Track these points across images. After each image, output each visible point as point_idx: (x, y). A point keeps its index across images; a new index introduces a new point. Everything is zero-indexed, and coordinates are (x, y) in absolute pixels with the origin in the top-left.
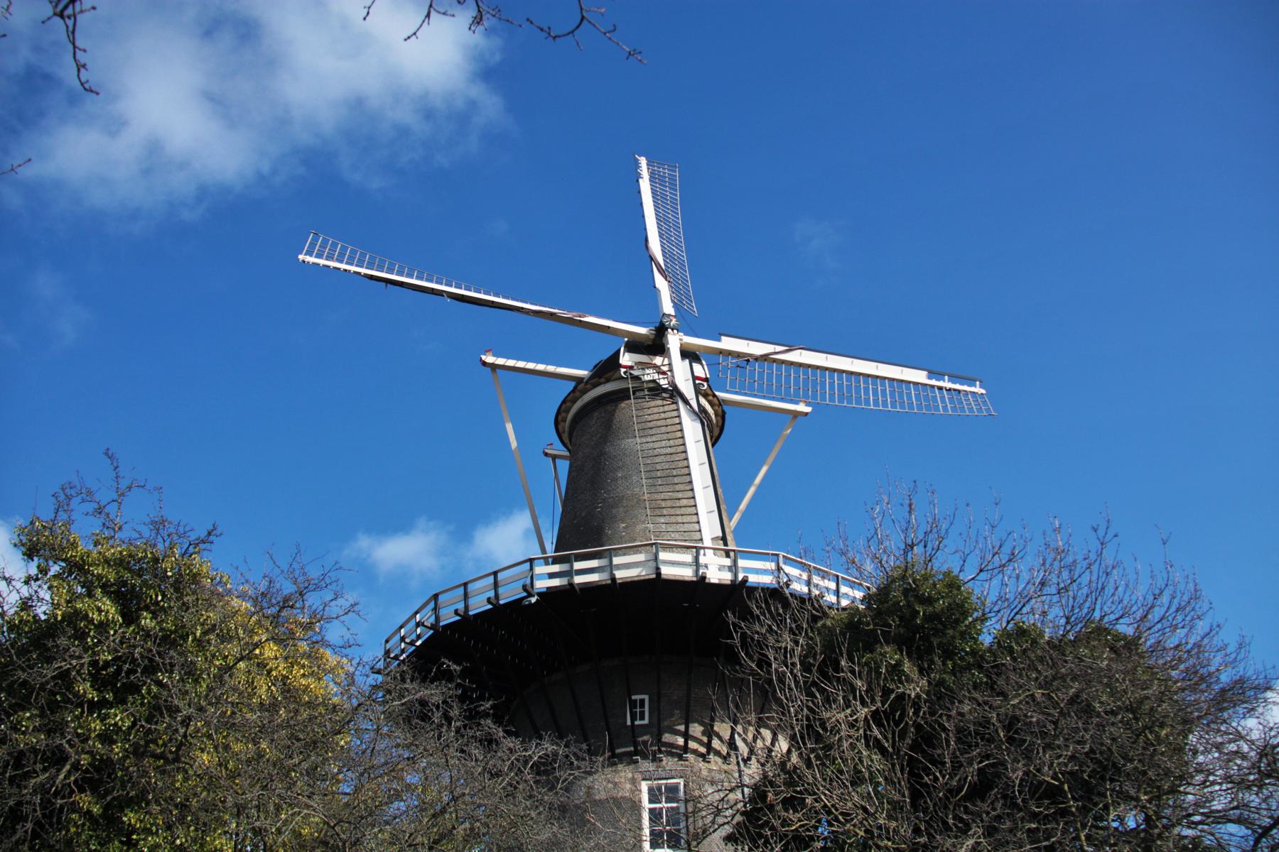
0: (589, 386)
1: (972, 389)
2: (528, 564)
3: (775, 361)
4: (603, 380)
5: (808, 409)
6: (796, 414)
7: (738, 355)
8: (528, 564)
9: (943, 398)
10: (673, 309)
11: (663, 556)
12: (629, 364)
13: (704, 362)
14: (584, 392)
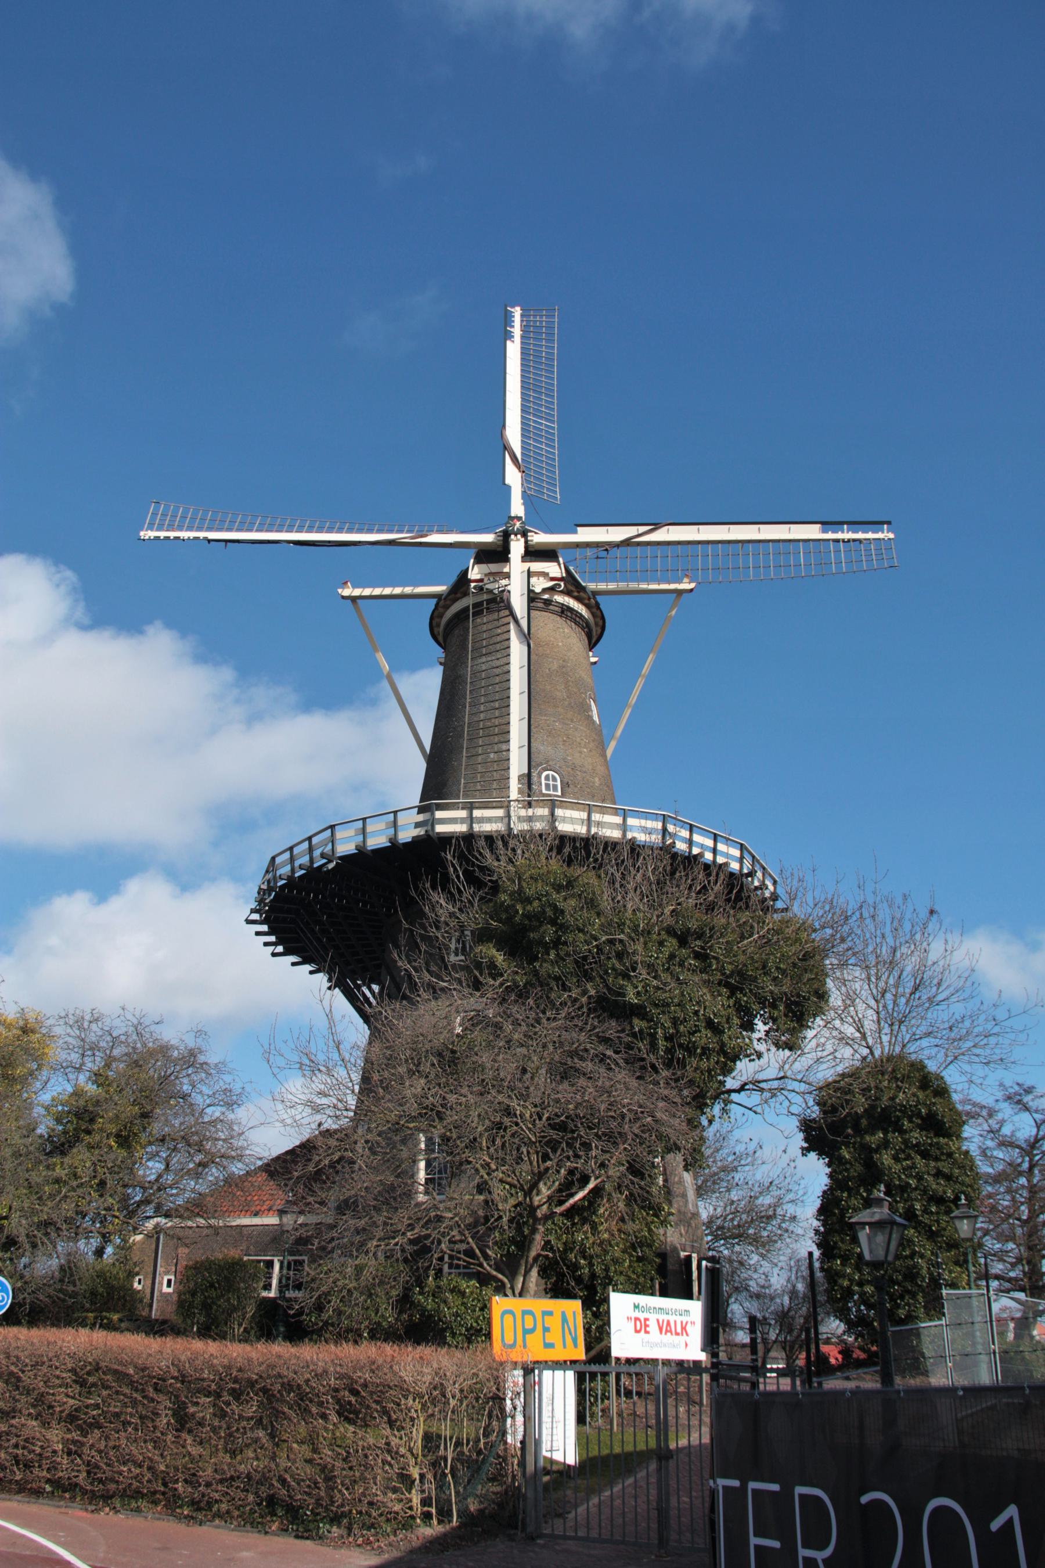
0: (448, 602)
1: (880, 535)
2: (329, 831)
3: (639, 544)
4: (459, 595)
5: (692, 586)
6: (679, 593)
7: (597, 545)
8: (329, 831)
9: (837, 551)
10: (523, 508)
11: (559, 812)
12: (478, 577)
13: (561, 560)
14: (447, 607)
